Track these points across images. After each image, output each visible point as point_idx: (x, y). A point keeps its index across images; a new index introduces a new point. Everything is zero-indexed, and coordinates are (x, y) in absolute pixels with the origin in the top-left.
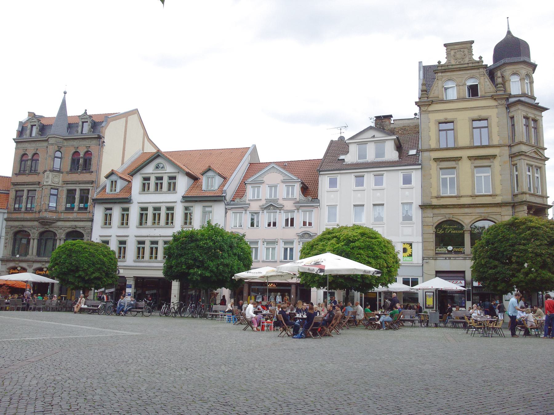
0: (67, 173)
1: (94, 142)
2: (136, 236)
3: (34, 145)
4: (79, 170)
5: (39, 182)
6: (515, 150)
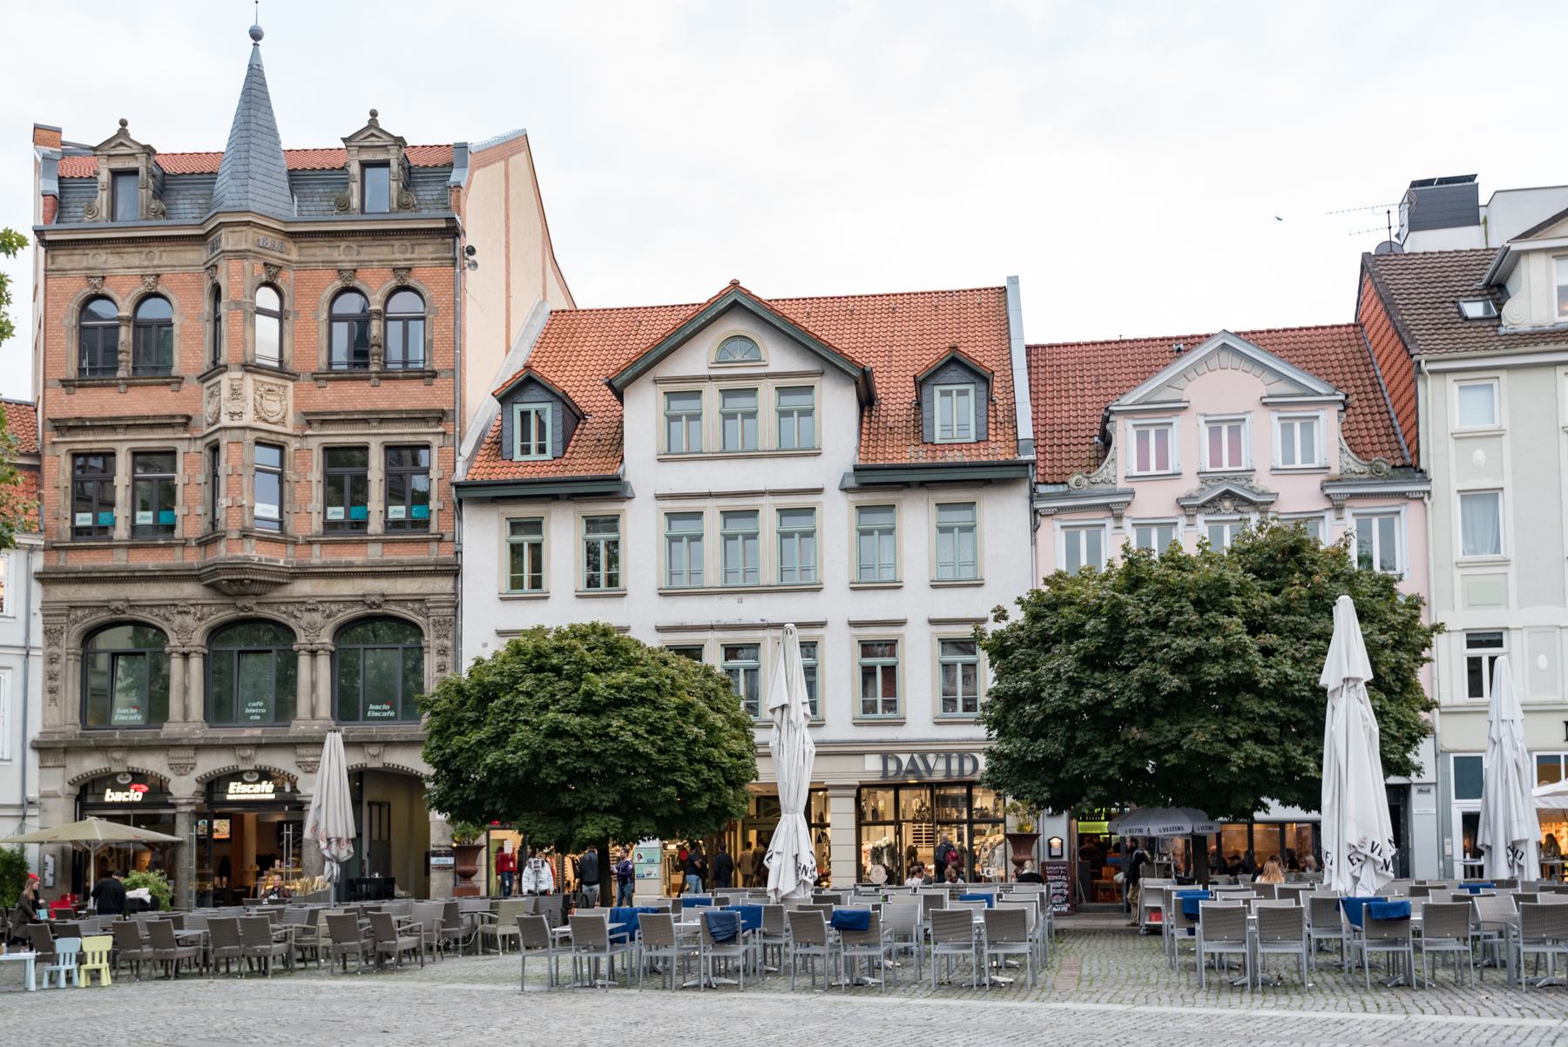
0: (316, 377)
1: (427, 250)
2: (853, 624)
3: (135, 258)
4: (120, 374)
5: (189, 418)
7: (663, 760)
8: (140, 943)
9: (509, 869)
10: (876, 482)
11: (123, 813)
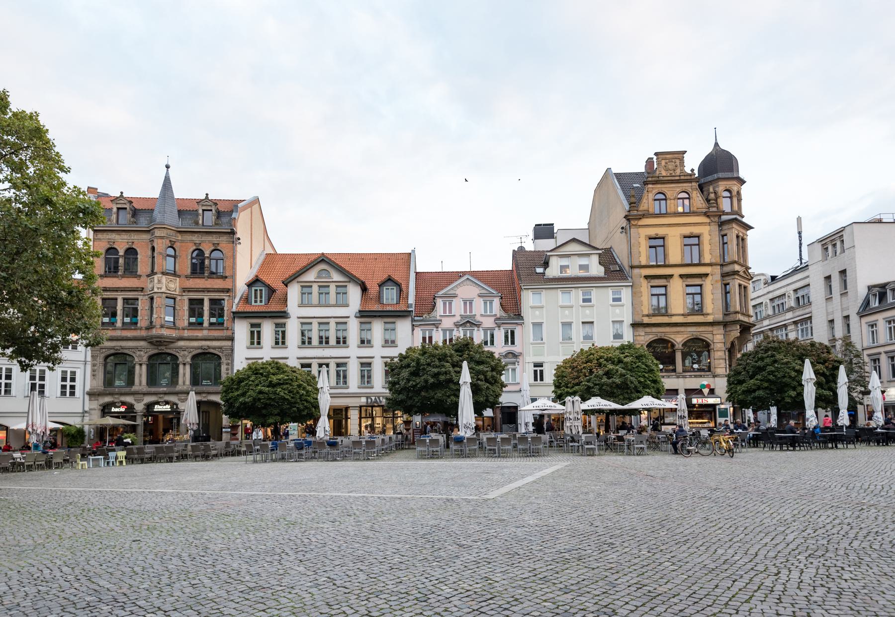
0: (187, 277)
1: (224, 239)
2: (358, 358)
3: (125, 236)
4: (120, 273)
6: (727, 269)
7: (293, 400)
8: (134, 454)
9: (248, 433)
10: (365, 315)
11: (118, 416)
